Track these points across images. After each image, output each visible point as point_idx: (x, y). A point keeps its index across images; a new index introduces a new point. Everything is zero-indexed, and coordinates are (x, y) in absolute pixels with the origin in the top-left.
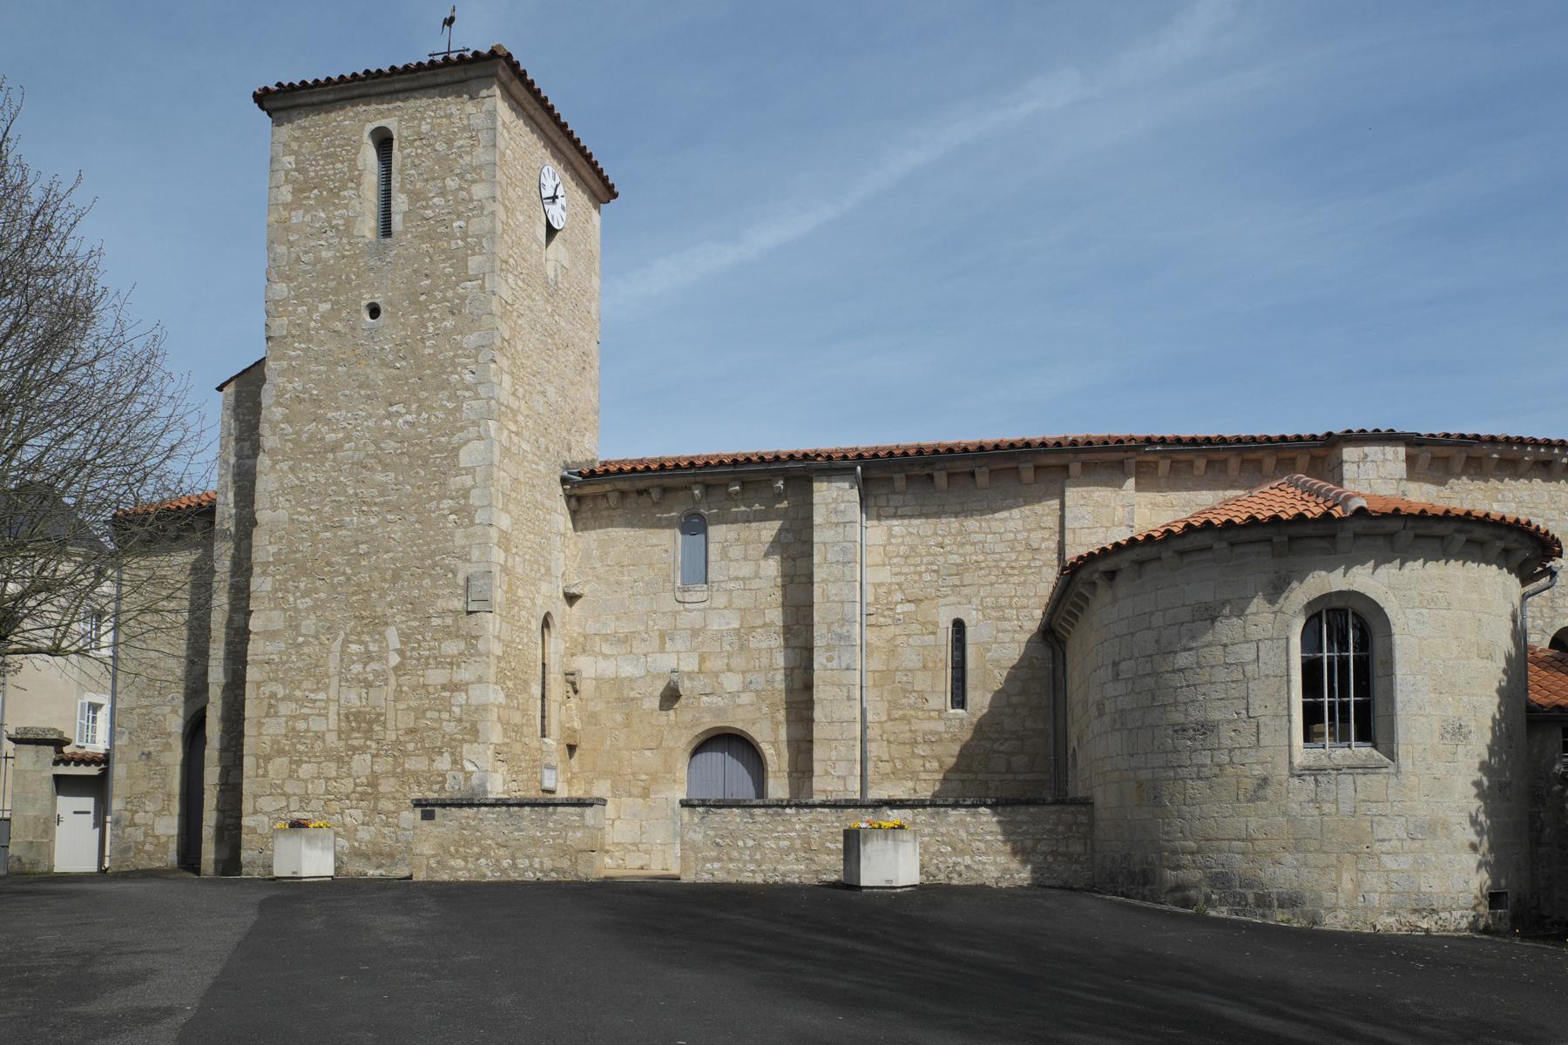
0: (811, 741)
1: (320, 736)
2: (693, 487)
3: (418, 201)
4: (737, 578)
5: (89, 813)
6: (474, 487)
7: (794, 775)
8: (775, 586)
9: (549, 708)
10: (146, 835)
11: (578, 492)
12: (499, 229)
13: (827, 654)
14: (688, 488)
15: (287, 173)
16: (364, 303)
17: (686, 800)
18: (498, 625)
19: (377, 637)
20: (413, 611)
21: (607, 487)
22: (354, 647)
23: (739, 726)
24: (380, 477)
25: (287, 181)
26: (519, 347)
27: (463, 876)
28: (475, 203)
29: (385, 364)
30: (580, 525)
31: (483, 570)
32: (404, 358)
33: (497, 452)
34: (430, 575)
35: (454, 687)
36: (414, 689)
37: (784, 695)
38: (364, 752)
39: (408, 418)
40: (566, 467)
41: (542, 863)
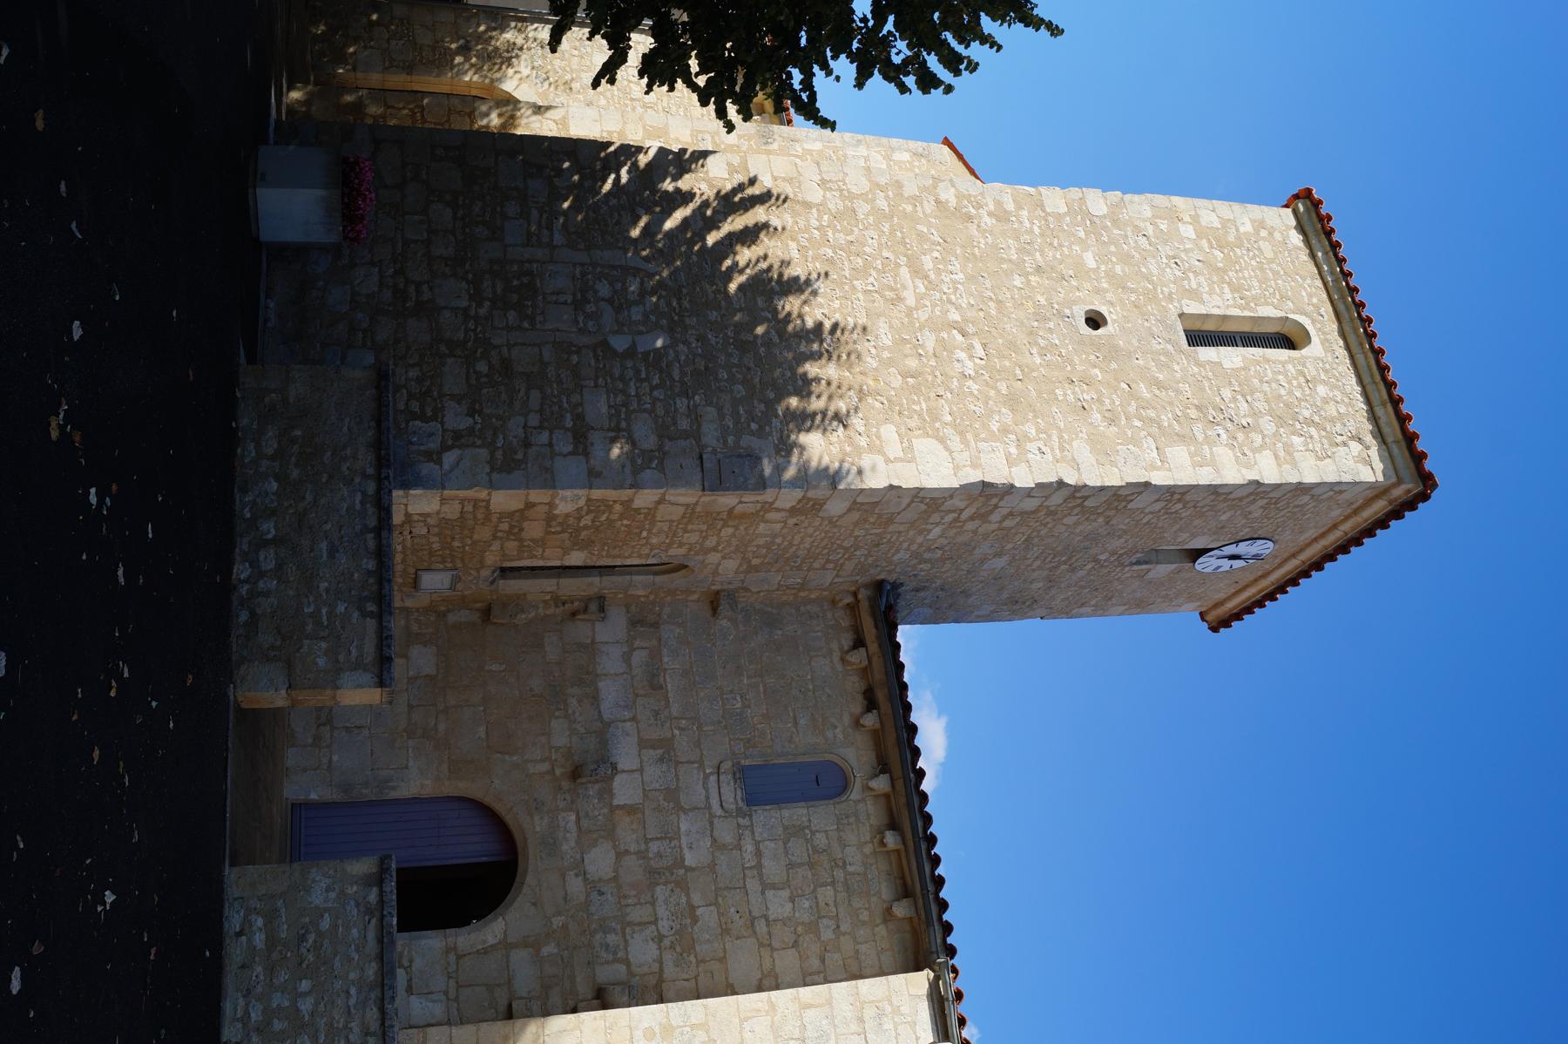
4: (758, 854)
9: (547, 577)
13: (657, 1030)
23: (530, 879)
41: (267, 594)
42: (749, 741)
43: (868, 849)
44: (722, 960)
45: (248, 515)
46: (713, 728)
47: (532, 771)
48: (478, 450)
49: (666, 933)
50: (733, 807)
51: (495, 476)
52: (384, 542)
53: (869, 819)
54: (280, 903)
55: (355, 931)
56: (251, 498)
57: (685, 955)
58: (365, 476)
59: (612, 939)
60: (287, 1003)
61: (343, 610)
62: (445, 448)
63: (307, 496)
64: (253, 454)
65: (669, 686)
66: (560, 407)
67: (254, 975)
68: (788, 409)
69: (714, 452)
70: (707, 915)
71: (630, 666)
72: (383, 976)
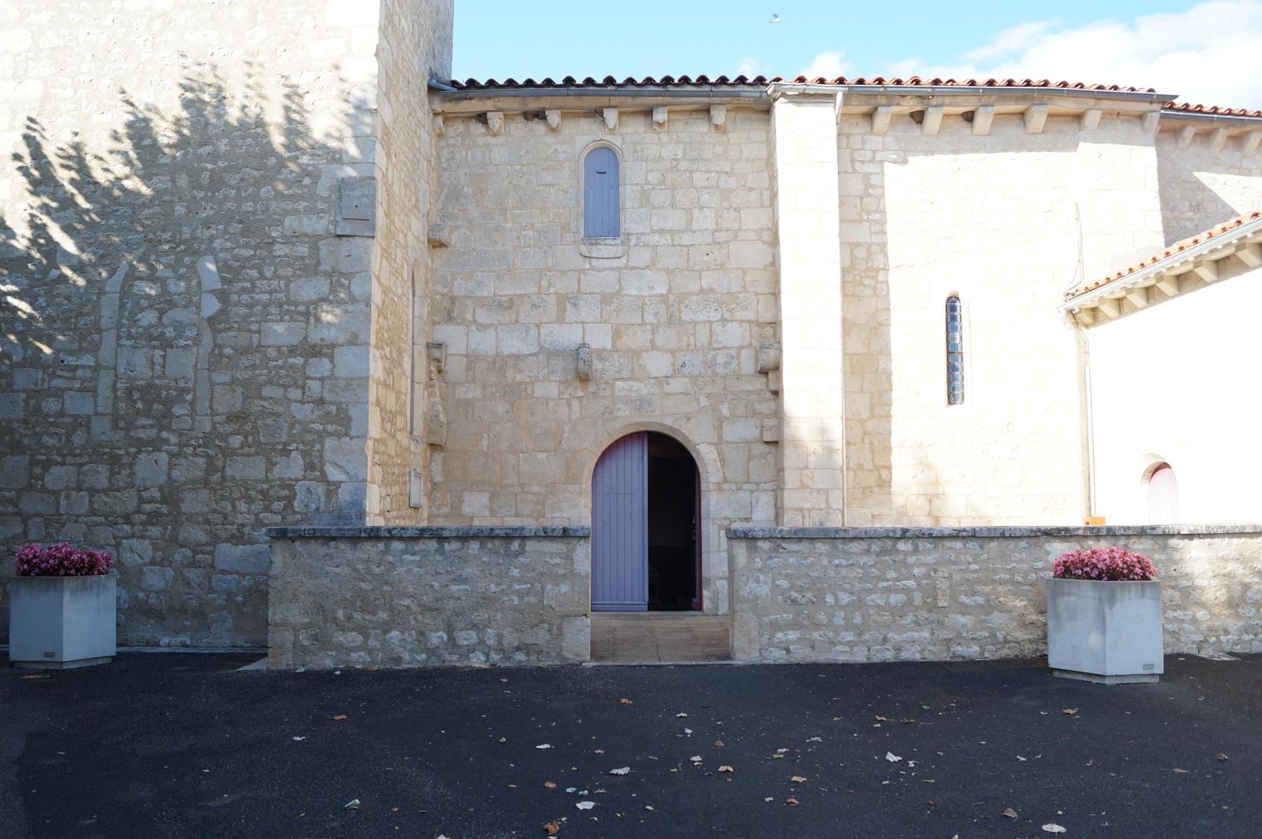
4: (661, 231)
23: (668, 422)
41: (500, 637)
42: (563, 228)
43: (665, 138)
44: (745, 271)
45: (424, 656)
46: (550, 259)
47: (578, 415)
48: (326, 447)
50: (620, 248)
51: (353, 432)
52: (454, 534)
53: (639, 134)
54: (766, 619)
55: (791, 560)
56: (407, 654)
57: (738, 301)
59: (721, 359)
60: (842, 613)
61: (517, 571)
62: (323, 477)
63: (406, 604)
64: (362, 653)
65: (509, 293)
66: (281, 368)
67: (819, 638)
68: (284, 145)
69: (335, 223)
70: (708, 280)
71: (491, 325)
72: (826, 538)
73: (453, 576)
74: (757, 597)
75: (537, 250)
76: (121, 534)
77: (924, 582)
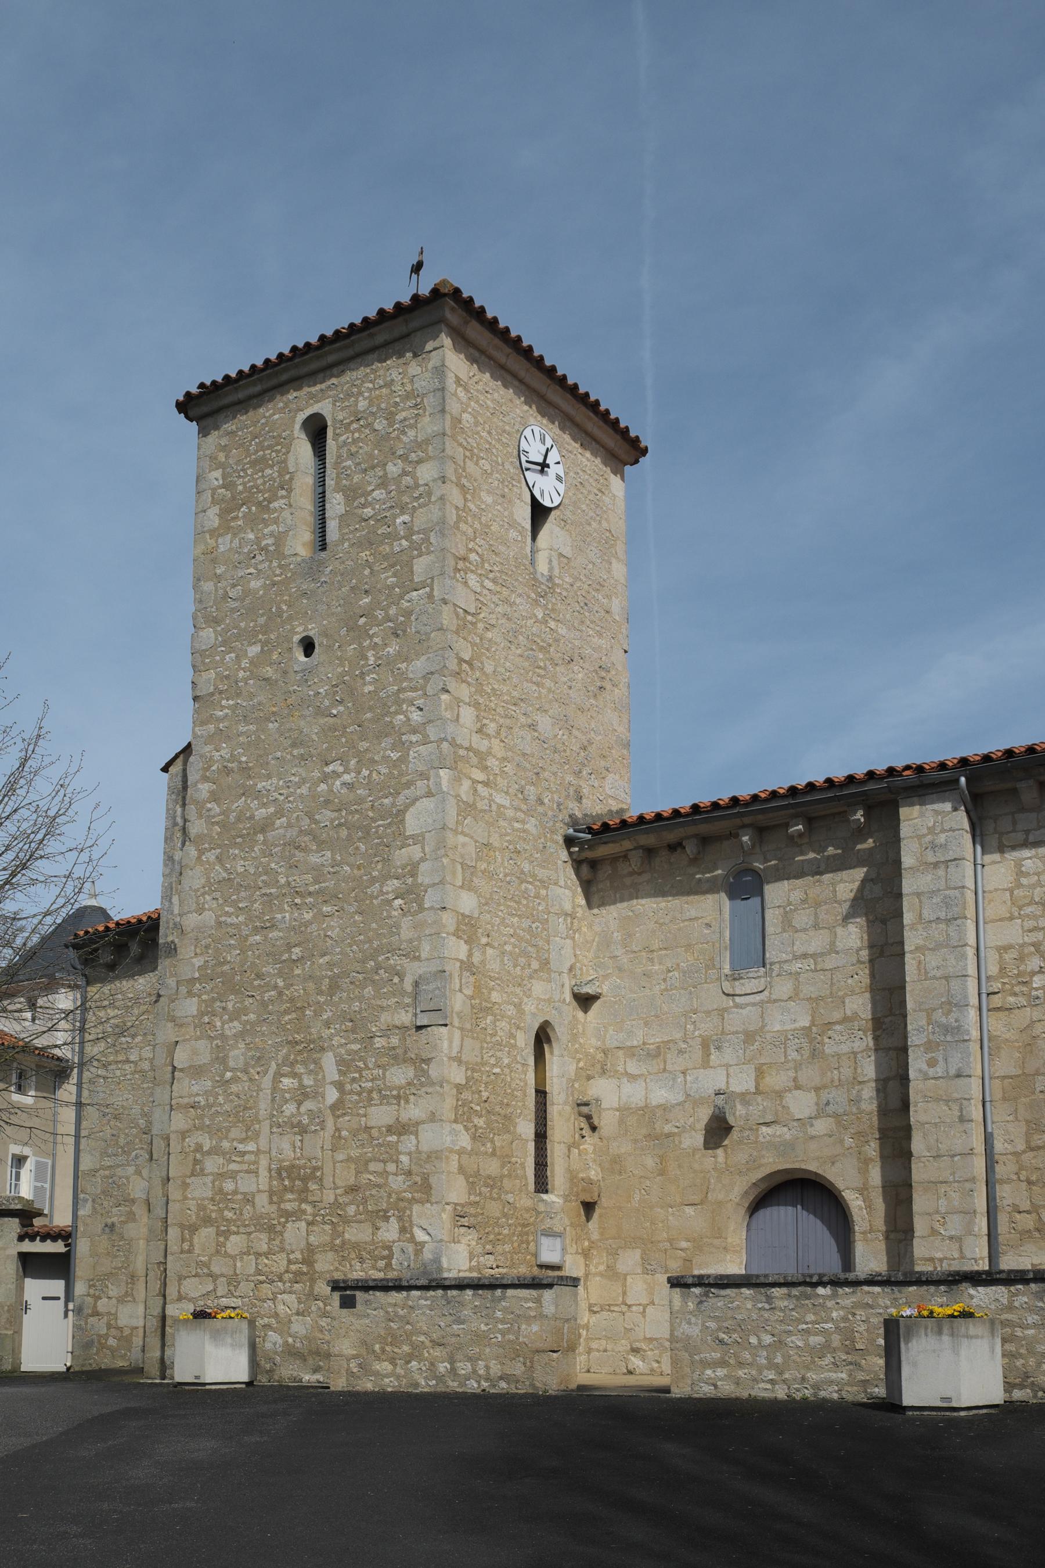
0: (911, 1186)
1: (249, 1199)
2: (740, 832)
3: (355, 499)
4: (805, 956)
5: (58, 1298)
6: (423, 860)
7: (892, 1236)
8: (859, 962)
10: (109, 1326)
11: (589, 854)
12: (452, 516)
13: (930, 1055)
14: (734, 835)
15: (214, 490)
16: (297, 638)
17: (677, 1278)
18: (457, 1042)
19: (312, 1067)
20: (354, 1031)
21: (627, 845)
22: (287, 1082)
23: (812, 1167)
24: (314, 859)
25: (214, 502)
26: (489, 669)
27: (390, 1384)
28: (421, 489)
29: (320, 712)
30: (595, 899)
31: (434, 969)
32: (341, 702)
33: (452, 812)
34: (373, 981)
35: (401, 1129)
36: (354, 1134)
37: (875, 1119)
38: (299, 1219)
39: (347, 778)
40: (574, 822)
41: (487, 1367)
45: (434, 1382)
48: (414, 1213)
49: (865, 1044)
58: (408, 1298)
62: (412, 1239)
64: (392, 1379)
73: (454, 1318)
74: (689, 1337)
75: (682, 991)
76: (277, 1290)
77: (842, 1325)
